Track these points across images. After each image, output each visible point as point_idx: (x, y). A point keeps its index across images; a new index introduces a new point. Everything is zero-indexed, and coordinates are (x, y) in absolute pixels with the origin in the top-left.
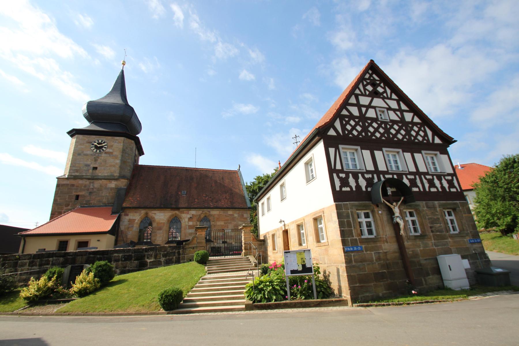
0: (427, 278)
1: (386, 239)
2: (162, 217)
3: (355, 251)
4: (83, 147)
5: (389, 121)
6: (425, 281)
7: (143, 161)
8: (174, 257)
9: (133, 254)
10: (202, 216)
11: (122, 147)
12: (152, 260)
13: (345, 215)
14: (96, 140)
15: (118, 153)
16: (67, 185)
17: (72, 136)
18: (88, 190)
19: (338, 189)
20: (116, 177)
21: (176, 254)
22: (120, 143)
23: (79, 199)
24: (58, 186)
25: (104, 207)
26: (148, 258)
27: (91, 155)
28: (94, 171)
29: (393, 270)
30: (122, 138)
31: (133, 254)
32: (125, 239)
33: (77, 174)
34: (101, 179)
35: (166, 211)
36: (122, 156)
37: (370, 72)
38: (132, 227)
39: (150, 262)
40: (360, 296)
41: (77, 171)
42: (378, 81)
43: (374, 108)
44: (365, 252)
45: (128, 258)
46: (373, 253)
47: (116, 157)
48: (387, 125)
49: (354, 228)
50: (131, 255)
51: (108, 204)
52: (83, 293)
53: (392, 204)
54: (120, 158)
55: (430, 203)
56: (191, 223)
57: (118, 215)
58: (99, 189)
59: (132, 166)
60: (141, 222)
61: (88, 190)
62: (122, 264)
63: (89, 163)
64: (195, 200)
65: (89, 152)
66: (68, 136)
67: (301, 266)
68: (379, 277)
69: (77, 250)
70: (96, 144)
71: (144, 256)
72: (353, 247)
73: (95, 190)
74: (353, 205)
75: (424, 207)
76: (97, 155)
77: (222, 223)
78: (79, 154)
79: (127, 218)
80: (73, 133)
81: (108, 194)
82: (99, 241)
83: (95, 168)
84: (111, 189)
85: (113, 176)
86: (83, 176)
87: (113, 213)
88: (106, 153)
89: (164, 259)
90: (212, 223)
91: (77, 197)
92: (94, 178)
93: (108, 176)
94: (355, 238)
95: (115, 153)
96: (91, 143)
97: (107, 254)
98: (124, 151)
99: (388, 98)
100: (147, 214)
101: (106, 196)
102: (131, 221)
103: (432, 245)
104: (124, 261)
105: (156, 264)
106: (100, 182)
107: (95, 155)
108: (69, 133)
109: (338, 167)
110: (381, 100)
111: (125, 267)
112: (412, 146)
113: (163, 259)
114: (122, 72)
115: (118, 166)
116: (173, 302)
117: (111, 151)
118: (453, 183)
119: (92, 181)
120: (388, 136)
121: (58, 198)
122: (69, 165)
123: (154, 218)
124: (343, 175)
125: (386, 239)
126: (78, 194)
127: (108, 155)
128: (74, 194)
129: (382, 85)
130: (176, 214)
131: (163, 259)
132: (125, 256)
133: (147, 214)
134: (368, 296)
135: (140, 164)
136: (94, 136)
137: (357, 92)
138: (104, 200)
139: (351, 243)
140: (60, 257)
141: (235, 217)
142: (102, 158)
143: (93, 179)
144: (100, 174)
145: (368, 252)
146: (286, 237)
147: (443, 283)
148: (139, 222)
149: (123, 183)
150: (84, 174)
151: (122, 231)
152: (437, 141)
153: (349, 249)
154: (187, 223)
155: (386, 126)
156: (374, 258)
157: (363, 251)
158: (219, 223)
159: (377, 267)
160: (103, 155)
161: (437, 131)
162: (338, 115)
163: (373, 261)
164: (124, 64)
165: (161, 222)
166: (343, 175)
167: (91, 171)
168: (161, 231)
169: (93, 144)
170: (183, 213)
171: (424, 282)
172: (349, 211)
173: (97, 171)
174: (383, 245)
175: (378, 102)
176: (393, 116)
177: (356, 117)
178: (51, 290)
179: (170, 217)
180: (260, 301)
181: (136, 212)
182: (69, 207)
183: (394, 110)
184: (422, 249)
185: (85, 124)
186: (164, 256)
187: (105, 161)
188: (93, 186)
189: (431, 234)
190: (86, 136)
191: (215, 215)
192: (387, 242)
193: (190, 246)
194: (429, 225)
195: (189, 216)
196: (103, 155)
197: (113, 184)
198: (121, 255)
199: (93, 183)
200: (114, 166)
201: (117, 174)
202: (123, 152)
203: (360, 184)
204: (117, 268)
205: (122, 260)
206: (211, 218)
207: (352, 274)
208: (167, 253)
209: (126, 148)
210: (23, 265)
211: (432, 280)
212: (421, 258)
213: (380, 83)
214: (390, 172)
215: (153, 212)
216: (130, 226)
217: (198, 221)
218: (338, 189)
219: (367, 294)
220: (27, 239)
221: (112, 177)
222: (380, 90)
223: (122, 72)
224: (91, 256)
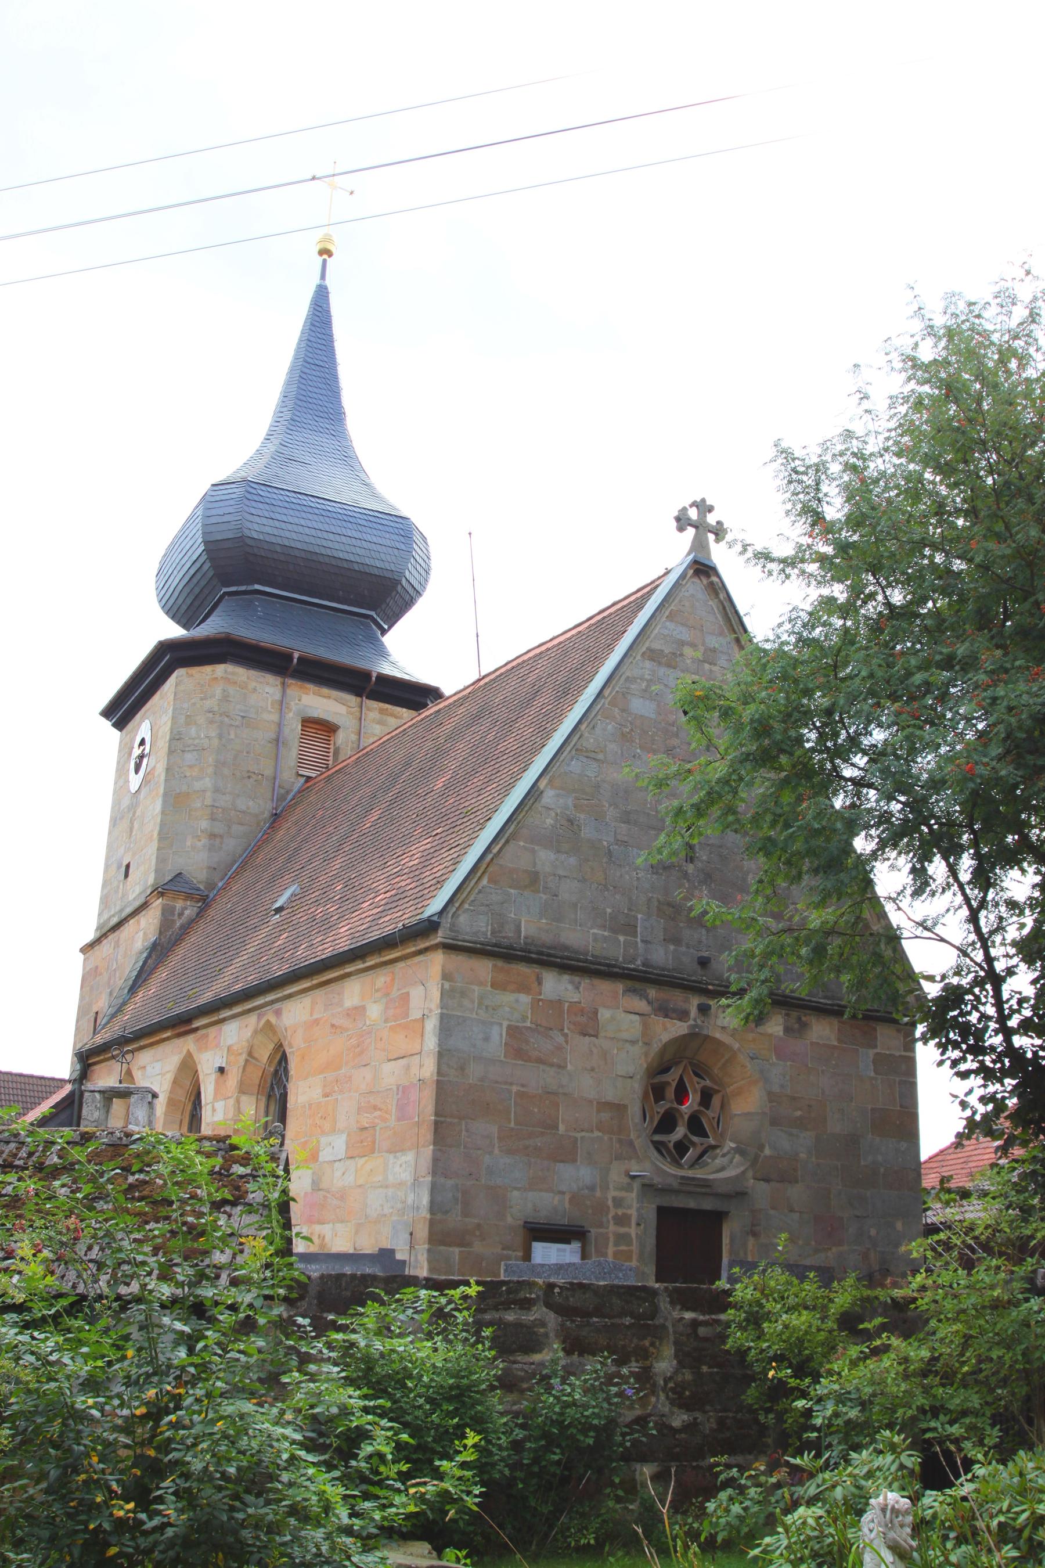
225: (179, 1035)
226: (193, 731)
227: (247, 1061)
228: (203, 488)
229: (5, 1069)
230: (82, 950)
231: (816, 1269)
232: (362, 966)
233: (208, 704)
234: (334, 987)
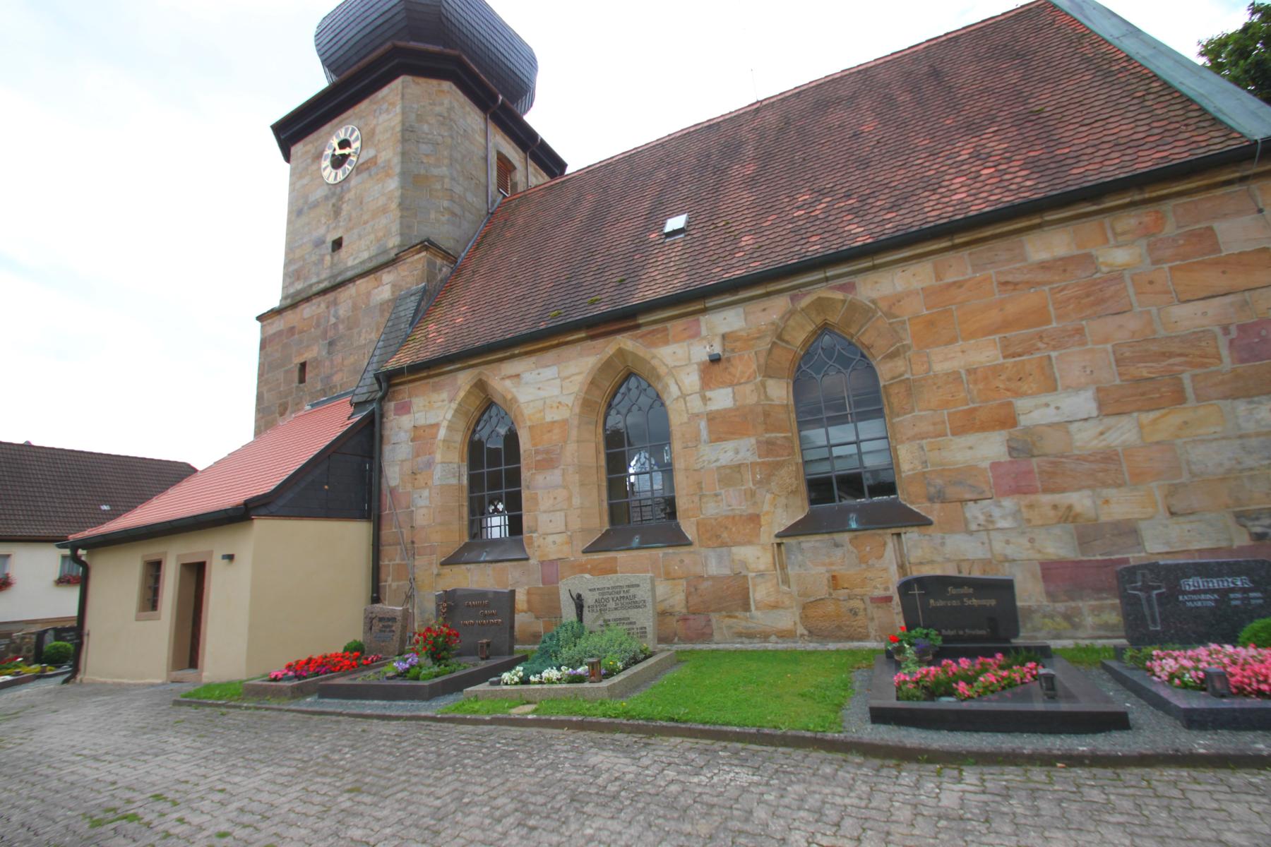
2: (552, 391)
10: (799, 336)
34: (352, 280)
35: (566, 352)
36: (403, 154)
38: (430, 464)
54: (397, 169)
56: (722, 399)
64: (737, 239)
73: (341, 327)
77: (985, 354)
79: (406, 421)
83: (337, 244)
85: (385, 252)
90: (885, 371)
93: (370, 259)
98: (408, 134)
100: (481, 386)
102: (422, 436)
106: (352, 290)
115: (394, 206)
119: (330, 296)
123: (514, 400)
128: (298, 360)
130: (621, 353)
133: (481, 386)
141: (1116, 276)
144: (350, 263)
146: (151, 582)
151: (392, 491)
154: (695, 404)
158: (946, 360)
168: (555, 476)
179: (593, 383)
181: (436, 388)
191: (898, 299)
195: (701, 352)
199: (335, 303)
201: (394, 242)
202: (404, 140)
206: (870, 336)
209: (420, 118)
215: (510, 368)
216: (423, 459)
217: (768, 371)
225: (592, 338)
226: (426, 127)
227: (774, 344)
228: (313, 31)
229: (15, 435)
230: (260, 318)
231: (800, 431)
232: (1137, 197)
233: (438, 109)
234: (1015, 239)
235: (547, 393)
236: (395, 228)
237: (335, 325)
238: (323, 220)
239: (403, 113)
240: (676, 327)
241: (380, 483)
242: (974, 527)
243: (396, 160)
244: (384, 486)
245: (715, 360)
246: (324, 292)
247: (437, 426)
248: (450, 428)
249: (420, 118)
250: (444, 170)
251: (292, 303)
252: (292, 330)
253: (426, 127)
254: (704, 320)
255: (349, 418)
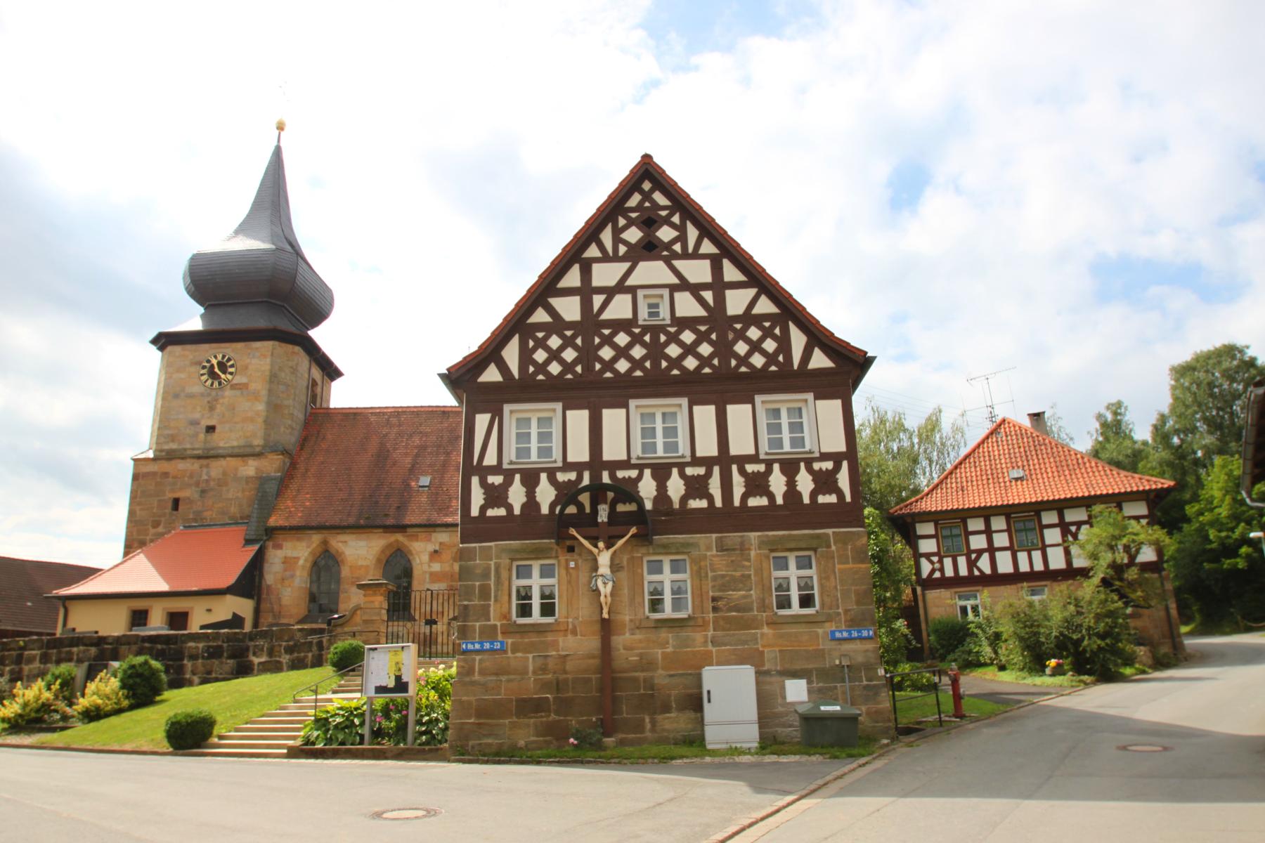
0: (659, 717)
1: (575, 627)
3: (487, 651)
4: (183, 376)
5: (668, 322)
6: (653, 723)
7: (341, 396)
8: (310, 655)
9: (225, 645)
11: (268, 367)
12: (263, 659)
13: (478, 571)
14: (213, 353)
15: (259, 386)
16: (154, 474)
17: (161, 349)
18: (197, 484)
19: (475, 512)
20: (258, 449)
21: (315, 648)
22: (265, 356)
23: (180, 508)
24: (136, 477)
25: (234, 527)
26: (254, 654)
27: (202, 395)
28: (209, 437)
29: (571, 694)
30: (269, 345)
31: (225, 645)
32: (276, 607)
33: (174, 446)
34: (224, 457)
36: (270, 391)
37: (647, 186)
38: (292, 576)
39: (260, 663)
40: (471, 743)
41: (173, 438)
42: (664, 208)
43: (633, 290)
44: (510, 654)
45: (215, 653)
46: (531, 656)
47: (256, 397)
48: (654, 336)
49: (496, 600)
50: (221, 647)
51: (242, 518)
52: (93, 715)
53: (596, 546)
54: (265, 399)
55: (734, 537)
56: (436, 567)
57: (257, 547)
58: (222, 483)
59: (301, 416)
60: (315, 564)
61: (197, 484)
62: (204, 665)
63: (197, 416)
65: (197, 389)
66: (154, 348)
67: (393, 678)
68: (528, 707)
69: (131, 630)
70: (214, 362)
71: (247, 649)
72: (481, 643)
73: (212, 483)
74: (504, 550)
75: (709, 548)
76: (214, 393)
78: (176, 396)
80: (164, 341)
81: (240, 495)
82: (209, 610)
83: (211, 429)
84: (248, 479)
85: (251, 446)
86: (185, 450)
87: (248, 542)
88: (234, 387)
89: (288, 657)
91: (176, 503)
92: (208, 456)
93: (239, 447)
94: (492, 622)
95: (253, 386)
96: (200, 363)
97: (175, 643)
98: (273, 378)
99: (685, 255)
100: (325, 543)
101: (236, 497)
102: (289, 562)
103: (706, 642)
104: (208, 658)
105: (273, 667)
106: (223, 463)
107: (209, 395)
108: (154, 342)
109: (490, 459)
110: (660, 264)
111: (209, 673)
112: (724, 386)
113: (285, 659)
114: (278, 153)
115: (260, 420)
116: (190, 737)
117: (244, 380)
118: (836, 481)
119: (204, 462)
120: (656, 364)
121: (138, 508)
122: (156, 426)
124: (496, 480)
125: (575, 627)
126: (176, 495)
127: (238, 393)
128: (171, 496)
129: (676, 219)
130: (397, 541)
131: (285, 659)
132: (209, 647)
133: (325, 543)
134: (490, 745)
135: (332, 405)
136: (206, 346)
137: (593, 251)
138: (234, 510)
139: (481, 633)
140: (92, 645)
142: (226, 401)
143: (207, 457)
144: (221, 444)
145: (519, 655)
147: (703, 730)
148: (308, 565)
149: (272, 465)
150: (188, 446)
151: (269, 587)
152: (819, 360)
153: (470, 647)
154: (425, 568)
155: (655, 338)
156: (531, 668)
157: (505, 652)
159: (530, 687)
160: (228, 393)
161: (819, 336)
162: (516, 324)
163: (527, 673)
164: (281, 127)
165: (360, 563)
166: (496, 480)
167: (202, 436)
169: (204, 367)
170: (415, 538)
171: (648, 726)
172: (492, 563)
173: (215, 436)
174: (561, 640)
175: (651, 272)
176: (687, 306)
177: (571, 325)
178: (46, 707)
179: (383, 552)
180: (342, 743)
181: (298, 539)
182: (161, 529)
183: (695, 289)
184: (670, 650)
185: (192, 318)
186: (289, 650)
187: (232, 408)
188: (208, 474)
189: (711, 615)
190: (189, 347)
192: (574, 633)
193: (346, 629)
194: (711, 594)
195: (431, 547)
196: (228, 393)
197: (250, 468)
198: (201, 645)
199: (207, 466)
200: (252, 420)
201: (258, 442)
202: (271, 382)
203: (538, 499)
204: (194, 673)
205: (203, 657)
207: (465, 698)
208: (295, 645)
209: (281, 369)
210: (30, 660)
211: (675, 722)
212: (660, 672)
213: (671, 215)
214: (633, 461)
216: (288, 573)
218: (475, 512)
219: (490, 741)
220: (70, 604)
221: (249, 450)
222: (666, 234)
223: (278, 153)
224: (147, 645)
226: (283, 375)
235: (360, 552)
236: (261, 433)
237: (207, 481)
238: (199, 409)
239: (272, 365)
240: (422, 535)
241: (260, 582)
242: (1102, 548)
243: (264, 393)
244: (264, 586)
245: (436, 551)
246: (199, 457)
247: (298, 558)
248: (306, 560)
249: (281, 369)
250: (290, 402)
251: (164, 455)
252: (166, 475)
253: (283, 375)
254: (434, 535)
255: (709, 692)
